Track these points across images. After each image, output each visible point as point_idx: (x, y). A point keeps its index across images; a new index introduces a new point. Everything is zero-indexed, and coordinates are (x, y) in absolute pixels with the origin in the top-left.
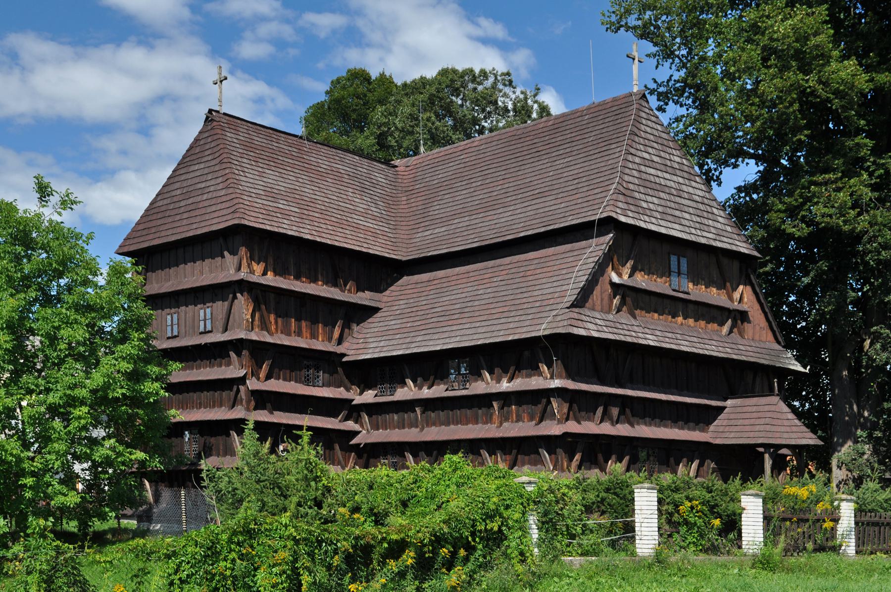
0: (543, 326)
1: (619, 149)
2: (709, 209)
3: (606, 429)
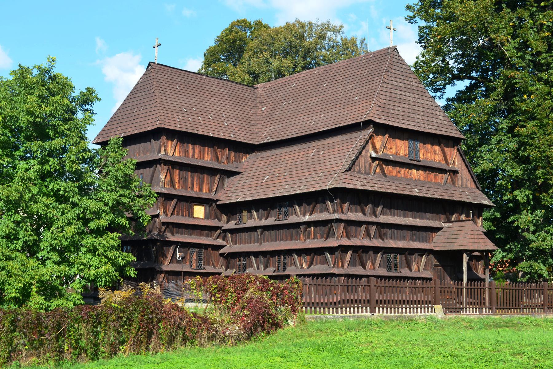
0: (329, 183)
1: (379, 80)
2: (434, 112)
3: (367, 242)
